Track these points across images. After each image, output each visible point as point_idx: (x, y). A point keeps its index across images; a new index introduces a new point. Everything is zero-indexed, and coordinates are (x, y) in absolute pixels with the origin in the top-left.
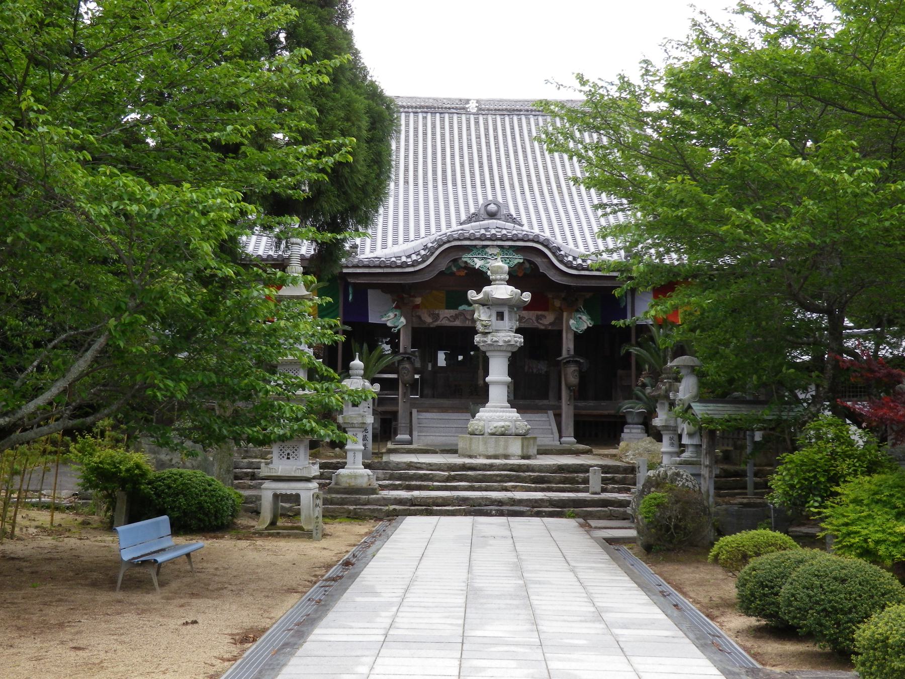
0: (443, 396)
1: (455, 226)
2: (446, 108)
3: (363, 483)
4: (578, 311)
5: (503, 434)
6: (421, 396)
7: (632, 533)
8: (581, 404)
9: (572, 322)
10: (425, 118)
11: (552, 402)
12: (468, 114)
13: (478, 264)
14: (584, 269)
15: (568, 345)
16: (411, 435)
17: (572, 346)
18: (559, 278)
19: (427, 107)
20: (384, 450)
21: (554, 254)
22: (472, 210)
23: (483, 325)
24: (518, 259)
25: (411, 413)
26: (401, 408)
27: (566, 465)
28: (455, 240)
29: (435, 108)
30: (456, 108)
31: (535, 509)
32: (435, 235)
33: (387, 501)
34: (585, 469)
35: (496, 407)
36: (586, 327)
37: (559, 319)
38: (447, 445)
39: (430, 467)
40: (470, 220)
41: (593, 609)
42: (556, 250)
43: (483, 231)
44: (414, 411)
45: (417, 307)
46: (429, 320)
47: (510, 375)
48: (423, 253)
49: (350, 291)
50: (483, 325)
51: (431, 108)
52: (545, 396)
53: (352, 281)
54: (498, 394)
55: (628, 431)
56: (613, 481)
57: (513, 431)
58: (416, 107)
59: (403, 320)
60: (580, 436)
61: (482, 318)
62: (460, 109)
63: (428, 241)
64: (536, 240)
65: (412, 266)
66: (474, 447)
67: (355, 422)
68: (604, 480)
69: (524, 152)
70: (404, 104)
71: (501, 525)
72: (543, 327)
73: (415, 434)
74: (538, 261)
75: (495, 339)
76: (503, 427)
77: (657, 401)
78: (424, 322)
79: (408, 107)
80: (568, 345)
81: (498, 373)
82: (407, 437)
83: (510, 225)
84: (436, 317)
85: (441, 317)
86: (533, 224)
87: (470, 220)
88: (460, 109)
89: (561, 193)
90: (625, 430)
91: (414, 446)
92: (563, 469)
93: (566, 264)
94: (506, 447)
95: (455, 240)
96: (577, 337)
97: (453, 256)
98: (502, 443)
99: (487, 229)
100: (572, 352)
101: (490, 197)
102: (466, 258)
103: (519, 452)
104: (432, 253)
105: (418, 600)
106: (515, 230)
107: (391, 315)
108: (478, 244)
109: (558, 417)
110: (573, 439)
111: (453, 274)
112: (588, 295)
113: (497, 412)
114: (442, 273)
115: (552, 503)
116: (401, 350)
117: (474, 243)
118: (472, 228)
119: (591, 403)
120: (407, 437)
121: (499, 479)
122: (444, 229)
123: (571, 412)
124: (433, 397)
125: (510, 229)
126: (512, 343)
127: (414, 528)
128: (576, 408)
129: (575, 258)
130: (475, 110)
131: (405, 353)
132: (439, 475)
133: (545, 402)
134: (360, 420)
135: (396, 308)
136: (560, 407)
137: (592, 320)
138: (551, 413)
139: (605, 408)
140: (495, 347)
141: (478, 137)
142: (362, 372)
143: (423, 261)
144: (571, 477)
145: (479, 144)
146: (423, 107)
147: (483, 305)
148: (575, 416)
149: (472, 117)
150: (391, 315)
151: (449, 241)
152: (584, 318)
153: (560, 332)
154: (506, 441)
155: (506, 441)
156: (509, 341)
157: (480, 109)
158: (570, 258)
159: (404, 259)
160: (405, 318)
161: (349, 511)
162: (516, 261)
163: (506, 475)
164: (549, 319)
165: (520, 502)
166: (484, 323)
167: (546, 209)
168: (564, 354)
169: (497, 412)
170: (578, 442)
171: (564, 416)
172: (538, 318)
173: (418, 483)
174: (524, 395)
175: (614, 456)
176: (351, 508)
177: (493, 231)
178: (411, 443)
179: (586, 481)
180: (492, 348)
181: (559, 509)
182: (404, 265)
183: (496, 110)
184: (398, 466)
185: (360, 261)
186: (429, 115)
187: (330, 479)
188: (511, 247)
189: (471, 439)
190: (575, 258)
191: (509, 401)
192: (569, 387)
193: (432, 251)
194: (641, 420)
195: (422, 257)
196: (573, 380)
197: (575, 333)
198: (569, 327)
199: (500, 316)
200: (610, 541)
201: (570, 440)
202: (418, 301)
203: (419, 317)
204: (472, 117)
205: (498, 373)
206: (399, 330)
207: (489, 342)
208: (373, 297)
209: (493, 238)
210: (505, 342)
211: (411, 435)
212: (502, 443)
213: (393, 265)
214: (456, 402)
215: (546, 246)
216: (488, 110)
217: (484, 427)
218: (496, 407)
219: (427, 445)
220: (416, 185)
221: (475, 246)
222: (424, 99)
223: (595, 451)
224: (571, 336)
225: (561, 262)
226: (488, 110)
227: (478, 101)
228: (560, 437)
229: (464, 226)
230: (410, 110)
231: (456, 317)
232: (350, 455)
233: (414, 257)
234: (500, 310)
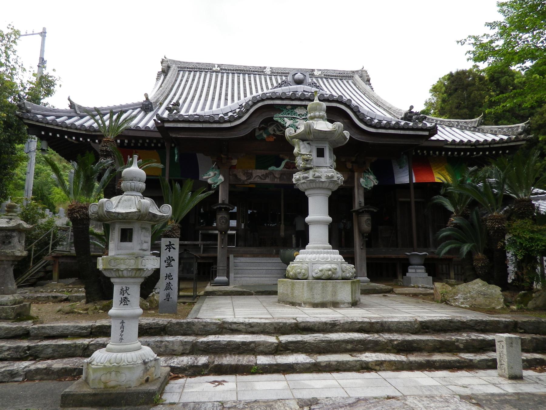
2: (252, 71)
5: (330, 278)
6: (237, 246)
9: (362, 180)
10: (238, 76)
12: (265, 75)
16: (228, 276)
17: (362, 200)
18: (359, 136)
19: (240, 70)
20: (202, 293)
23: (304, 160)
25: (228, 258)
26: (220, 253)
27: (431, 322)
29: (245, 71)
30: (258, 72)
35: (318, 248)
36: (372, 185)
38: (259, 286)
40: (276, 87)
44: (231, 257)
45: (234, 167)
46: (244, 178)
47: (330, 214)
49: (176, 152)
50: (304, 160)
51: (242, 71)
54: (318, 235)
55: (413, 271)
57: (339, 274)
58: (233, 70)
59: (221, 178)
61: (303, 152)
62: (260, 72)
63: (243, 100)
65: (229, 121)
66: (296, 293)
67: (123, 267)
70: (226, 68)
73: (232, 275)
75: (317, 174)
76: (330, 270)
78: (240, 180)
79: (229, 70)
81: (318, 212)
82: (225, 278)
84: (250, 176)
85: (254, 175)
88: (260, 72)
90: (410, 270)
92: (428, 328)
94: (335, 293)
96: (369, 195)
98: (330, 289)
100: (363, 205)
103: (349, 299)
107: (212, 174)
110: (366, 279)
111: (263, 140)
113: (318, 255)
116: (220, 202)
117: (285, 102)
120: (225, 278)
121: (349, 346)
122: (255, 94)
123: (364, 256)
124: (245, 246)
126: (335, 179)
128: (367, 253)
130: (269, 73)
131: (223, 203)
132: (264, 343)
134: (132, 264)
137: (377, 179)
140: (316, 184)
143: (240, 117)
146: (238, 70)
147: (303, 140)
148: (368, 259)
149: (268, 77)
152: (372, 177)
153: (352, 189)
154: (334, 287)
155: (334, 287)
156: (332, 177)
157: (273, 72)
160: (224, 176)
163: (360, 342)
166: (305, 157)
168: (357, 207)
169: (318, 255)
170: (372, 281)
174: (339, 239)
178: (227, 284)
180: (314, 185)
183: (282, 73)
186: (241, 75)
189: (293, 284)
191: (330, 242)
192: (361, 233)
194: (423, 262)
196: (367, 227)
197: (365, 189)
198: (360, 185)
199: (320, 153)
202: (234, 162)
203: (236, 176)
204: (268, 77)
205: (318, 212)
206: (218, 186)
207: (311, 178)
210: (328, 177)
211: (228, 276)
212: (330, 289)
215: (349, 106)
217: (307, 270)
218: (318, 248)
219: (243, 286)
222: (238, 66)
224: (362, 192)
226: (277, 73)
227: (271, 68)
230: (230, 72)
231: (266, 176)
234: (321, 146)
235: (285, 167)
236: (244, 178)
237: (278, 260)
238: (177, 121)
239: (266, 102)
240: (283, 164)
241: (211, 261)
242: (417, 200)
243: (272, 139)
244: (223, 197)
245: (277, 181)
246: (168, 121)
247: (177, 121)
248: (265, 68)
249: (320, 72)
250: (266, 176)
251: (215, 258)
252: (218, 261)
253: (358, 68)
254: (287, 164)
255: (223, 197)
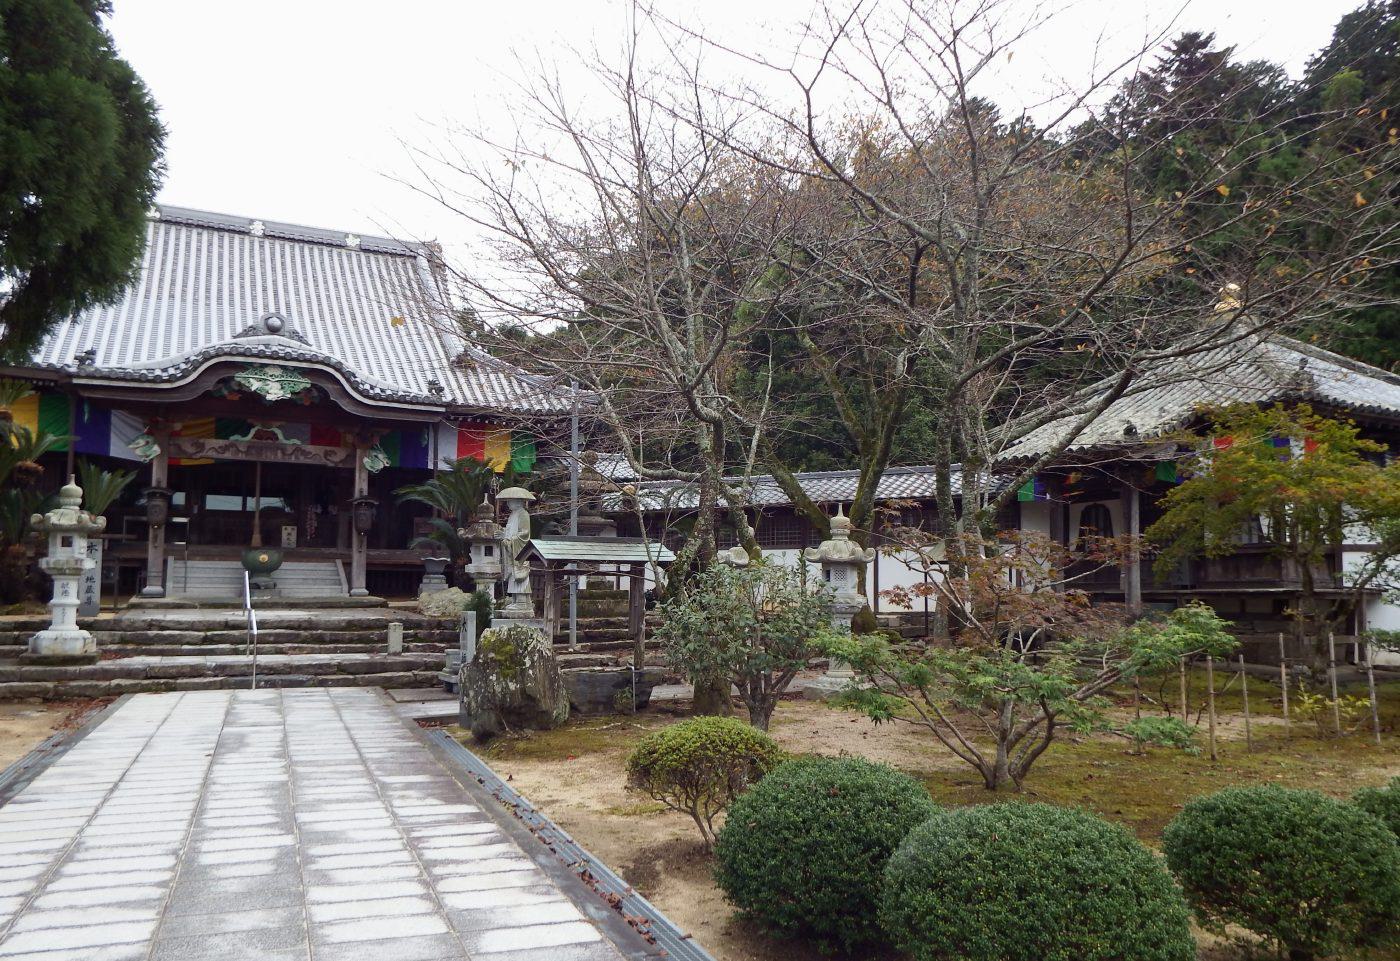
0: (210, 543)
1: (228, 339)
3: (77, 649)
4: (372, 448)
7: (452, 708)
8: (373, 553)
9: (366, 460)
11: (341, 550)
13: (255, 385)
14: (381, 400)
15: (361, 485)
16: (164, 586)
17: (365, 487)
21: (348, 380)
22: (250, 323)
24: (304, 383)
25: (165, 562)
26: (154, 555)
28: (226, 354)
31: (320, 677)
32: (202, 346)
33: (107, 675)
34: (383, 625)
37: (351, 457)
39: (179, 625)
40: (239, 336)
41: (438, 926)
42: (349, 376)
43: (262, 347)
44: (171, 560)
45: (177, 434)
46: (190, 450)
48: (183, 366)
52: (333, 544)
53: (86, 394)
56: (416, 638)
59: (156, 449)
60: (372, 587)
64: (326, 362)
68: (405, 637)
69: (315, 280)
71: (268, 703)
72: (331, 465)
73: (169, 585)
74: (328, 387)
77: (470, 545)
80: (361, 485)
82: (159, 589)
83: (295, 343)
84: (201, 447)
86: (323, 343)
87: (247, 332)
89: (355, 325)
91: (167, 600)
93: (361, 393)
95: (226, 354)
96: (373, 479)
97: (224, 374)
99: (267, 346)
100: (365, 493)
101: (272, 309)
102: (240, 377)
104: (195, 369)
105: (122, 829)
106: (304, 349)
107: (142, 442)
108: (256, 362)
109: (348, 565)
111: (223, 397)
112: (386, 431)
114: (207, 395)
115: (341, 668)
116: (154, 484)
118: (246, 342)
119: (384, 552)
120: (159, 589)
123: (364, 561)
124: (200, 543)
125: (295, 347)
127: (140, 711)
129: (372, 388)
131: (158, 487)
133: (333, 550)
135: (149, 433)
136: (350, 557)
138: (339, 562)
139: (399, 556)
141: (263, 261)
142: (80, 501)
143: (183, 377)
144: (368, 635)
145: (263, 267)
150: (142, 442)
151: (218, 355)
152: (380, 456)
153: (352, 472)
158: (367, 387)
159: (158, 372)
160: (160, 445)
161: (46, 691)
162: (302, 386)
164: (338, 456)
165: (299, 669)
167: (339, 339)
168: (357, 495)
171: (355, 564)
172: (326, 454)
173: (160, 647)
175: (414, 610)
176: (50, 685)
177: (274, 348)
178: (163, 595)
179: (384, 639)
181: (348, 676)
182: (157, 379)
184: (132, 626)
185: (97, 370)
187: (26, 644)
188: (296, 368)
190: (372, 388)
193: (196, 365)
195: (183, 371)
198: (363, 466)
200: (427, 722)
201: (360, 589)
202: (178, 426)
208: (117, 420)
209: (274, 356)
211: (164, 586)
213: (141, 379)
214: (227, 549)
215: (338, 370)
216: (276, 235)
220: (183, 300)
221: (251, 364)
223: (392, 604)
224: (365, 476)
225: (356, 389)
228: (350, 588)
229: (238, 340)
231: (225, 449)
232: (57, 612)
233: (172, 371)
235: (255, 436)
236: (190, 450)
237: (238, 564)
238: (89, 376)
239: (223, 359)
240: (253, 432)
241: (136, 565)
242: (256, 538)
243: (236, 398)
244: (158, 475)
245: (241, 457)
246: (78, 376)
247: (89, 376)
248: (252, 221)
249: (357, 241)
250: (225, 449)
251: (144, 562)
252: (150, 564)
253: (428, 239)
254: (258, 432)
255: (158, 475)
